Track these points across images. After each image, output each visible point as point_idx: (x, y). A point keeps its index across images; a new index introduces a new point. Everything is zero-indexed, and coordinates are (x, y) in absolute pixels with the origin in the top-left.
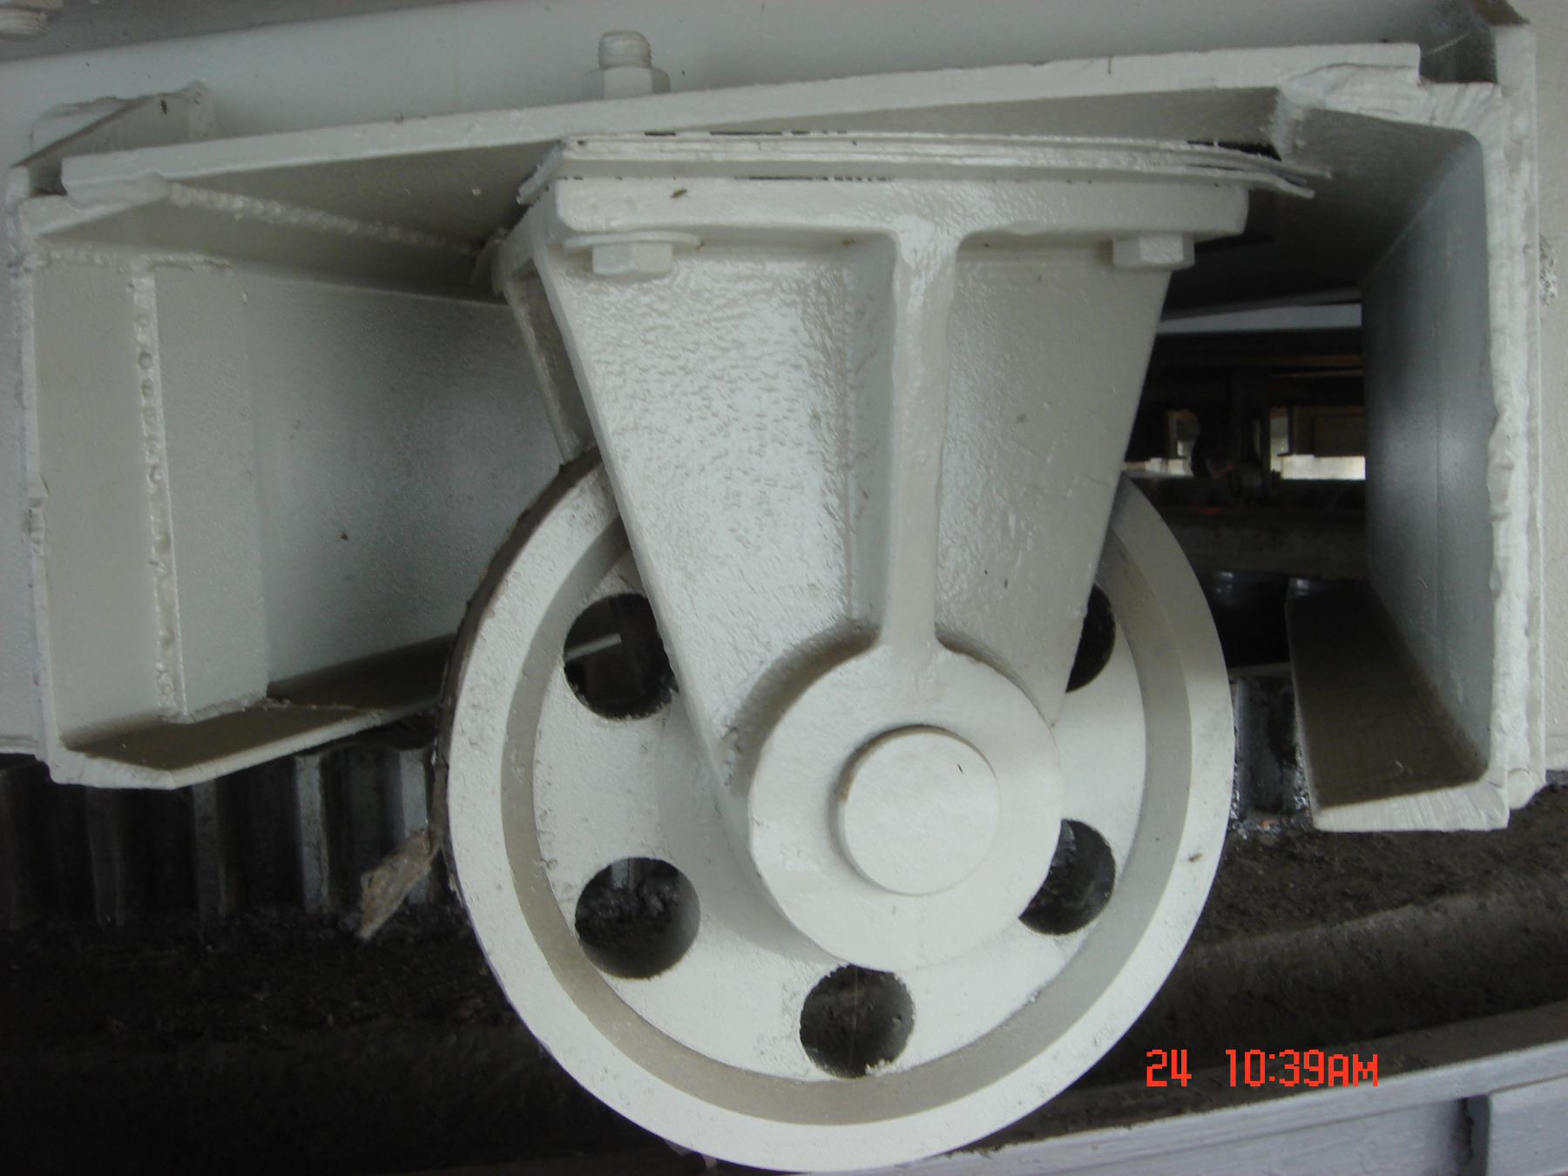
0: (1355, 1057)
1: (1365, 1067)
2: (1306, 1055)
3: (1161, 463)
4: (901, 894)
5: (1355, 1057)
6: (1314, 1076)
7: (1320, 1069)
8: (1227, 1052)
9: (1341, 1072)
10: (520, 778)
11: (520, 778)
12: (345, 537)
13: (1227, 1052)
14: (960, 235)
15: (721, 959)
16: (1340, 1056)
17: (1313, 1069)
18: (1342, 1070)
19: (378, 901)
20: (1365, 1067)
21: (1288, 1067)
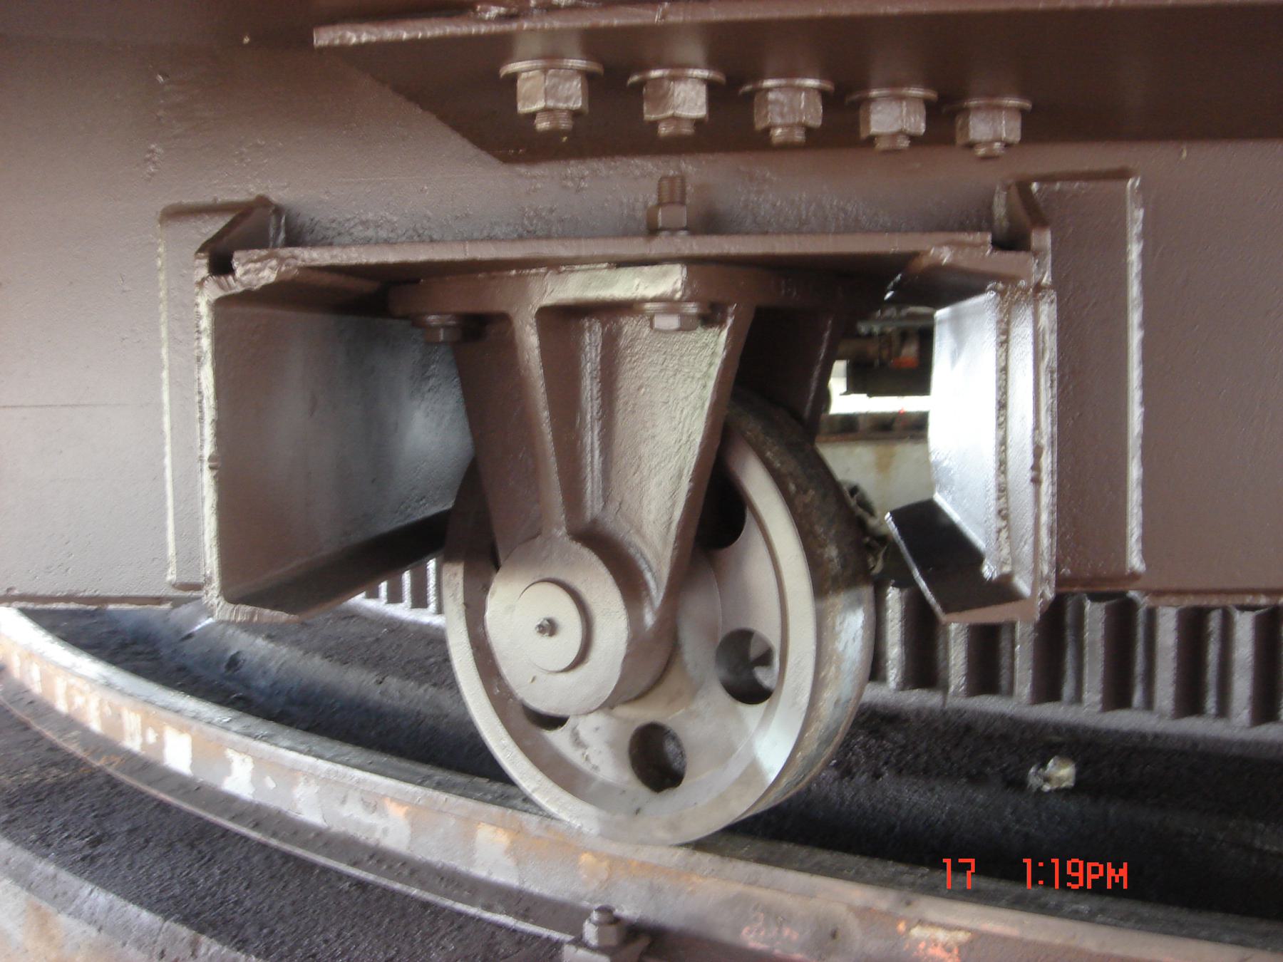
0: (1109, 865)
1: (1117, 873)
2: (1090, 865)
3: (120, 742)
4: (526, 589)
5: (1109, 865)
6: (1075, 880)
7: (1080, 874)
8: (1024, 860)
9: (385, 601)
10: (205, 575)
11: (205, 575)
12: (88, 367)
13: (1024, 860)
14: (160, 209)
15: (597, 729)
17: (1074, 874)
18: (1078, 872)
19: (194, 224)
20: (1117, 873)
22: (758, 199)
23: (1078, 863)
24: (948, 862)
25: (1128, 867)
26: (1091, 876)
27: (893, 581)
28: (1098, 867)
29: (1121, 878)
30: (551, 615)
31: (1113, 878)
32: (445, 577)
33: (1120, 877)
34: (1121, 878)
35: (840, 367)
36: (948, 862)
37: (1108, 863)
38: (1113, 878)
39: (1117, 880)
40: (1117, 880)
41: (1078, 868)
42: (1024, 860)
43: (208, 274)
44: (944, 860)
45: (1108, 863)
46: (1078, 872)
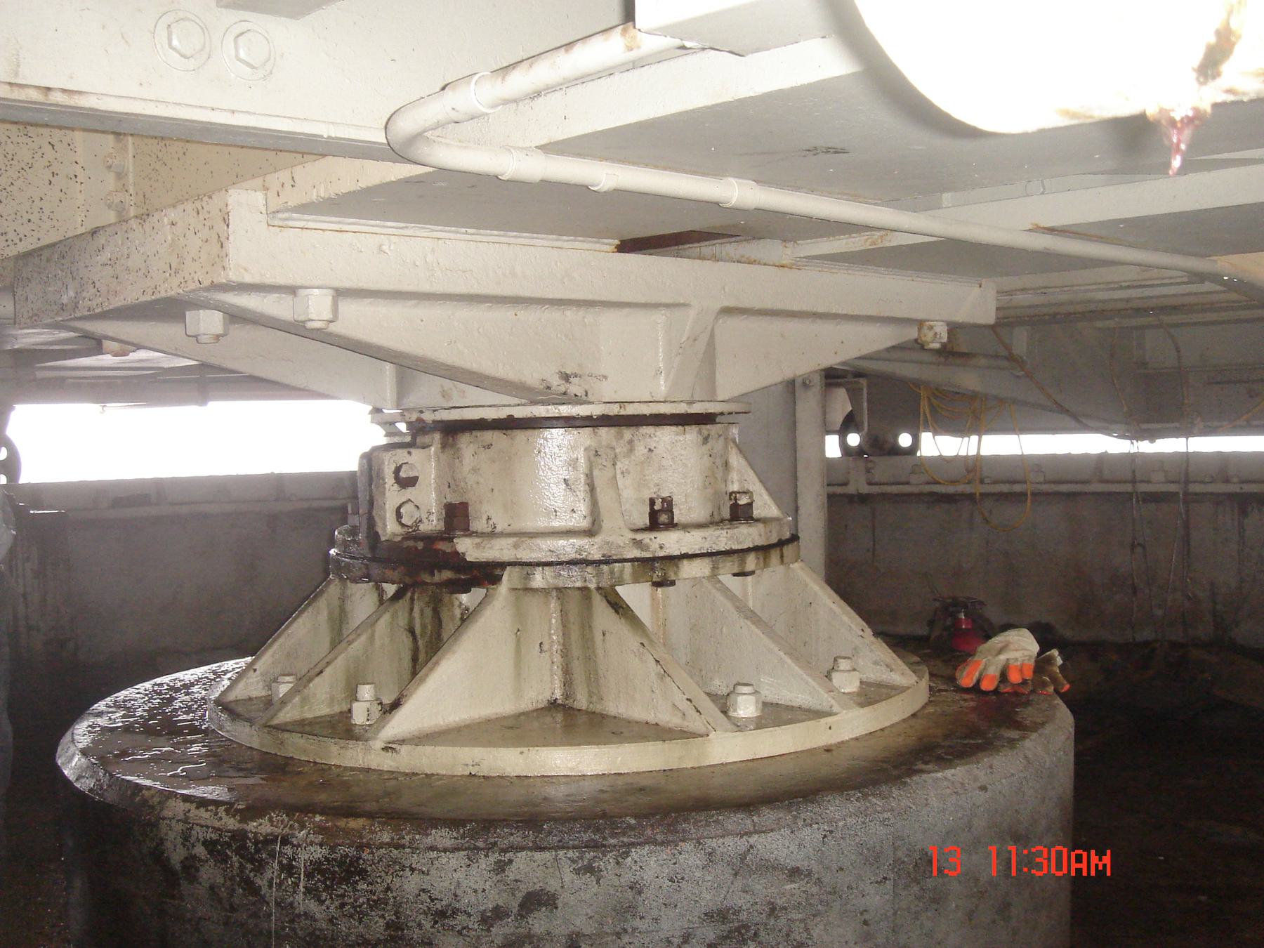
0: (1093, 852)
5: (1093, 852)
16: (1060, 848)
21: (1038, 860)
29: (1105, 866)
34: (1105, 866)
38: (1097, 865)
40: (1100, 868)
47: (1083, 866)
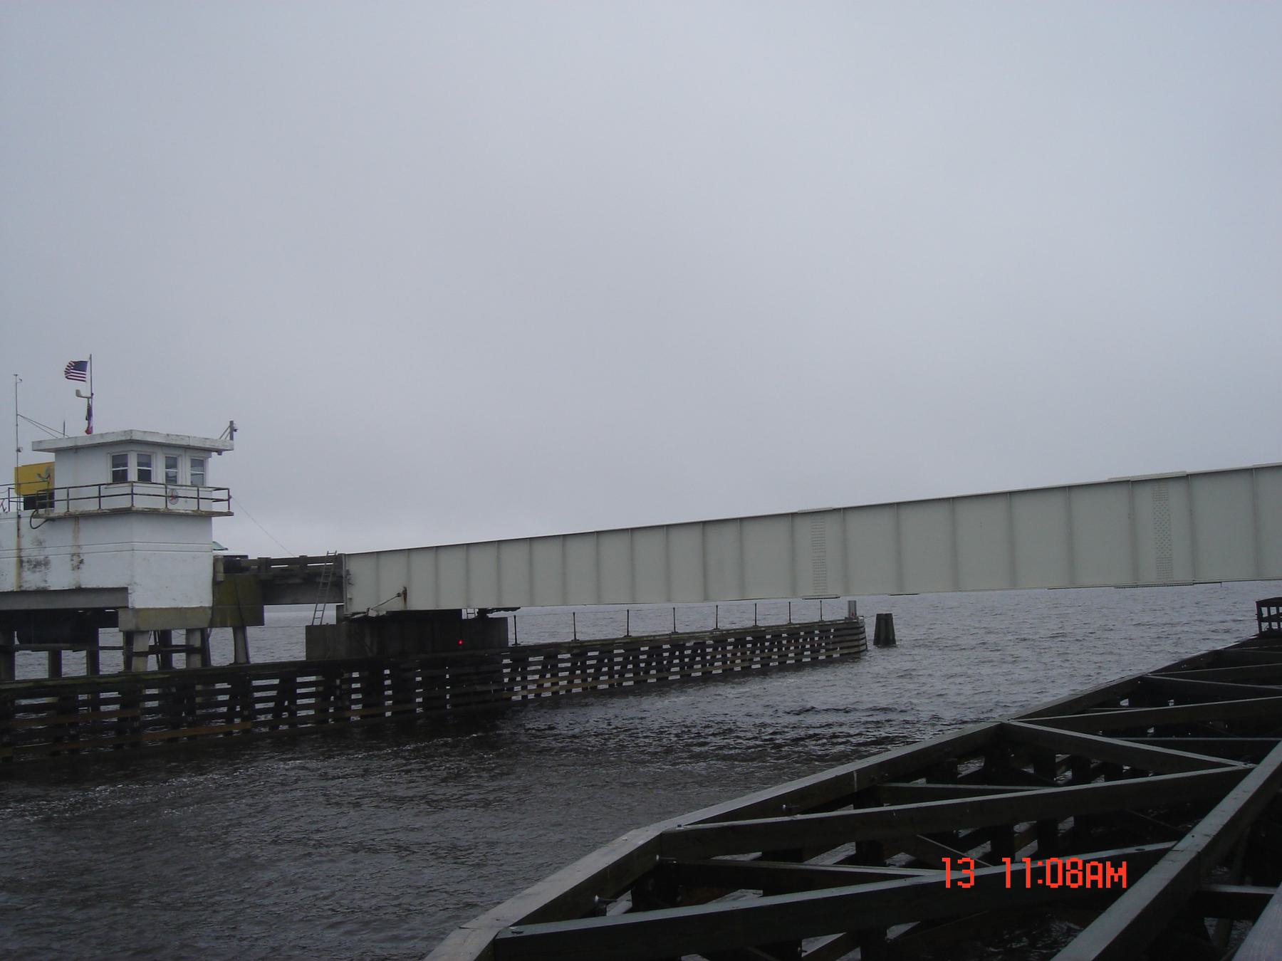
18: (1097, 874)
22: (93, 662)
23: (1097, 866)
24: (947, 861)
25: (1127, 866)
26: (1089, 878)
27: (960, 776)
28: (1097, 866)
29: (1120, 877)
30: (235, 514)
31: (1112, 877)
32: (207, 486)
33: (1119, 876)
34: (1120, 877)
35: (323, 679)
36: (947, 861)
37: (1107, 862)
38: (1112, 877)
39: (1116, 880)
40: (1116, 880)
41: (1094, 874)
42: (943, 860)
43: (191, 643)
44: (943, 860)
45: (1107, 862)
46: (1097, 874)
47: (1099, 877)
